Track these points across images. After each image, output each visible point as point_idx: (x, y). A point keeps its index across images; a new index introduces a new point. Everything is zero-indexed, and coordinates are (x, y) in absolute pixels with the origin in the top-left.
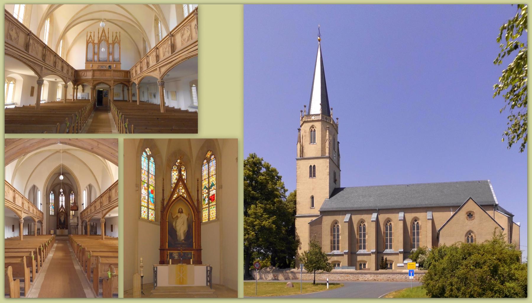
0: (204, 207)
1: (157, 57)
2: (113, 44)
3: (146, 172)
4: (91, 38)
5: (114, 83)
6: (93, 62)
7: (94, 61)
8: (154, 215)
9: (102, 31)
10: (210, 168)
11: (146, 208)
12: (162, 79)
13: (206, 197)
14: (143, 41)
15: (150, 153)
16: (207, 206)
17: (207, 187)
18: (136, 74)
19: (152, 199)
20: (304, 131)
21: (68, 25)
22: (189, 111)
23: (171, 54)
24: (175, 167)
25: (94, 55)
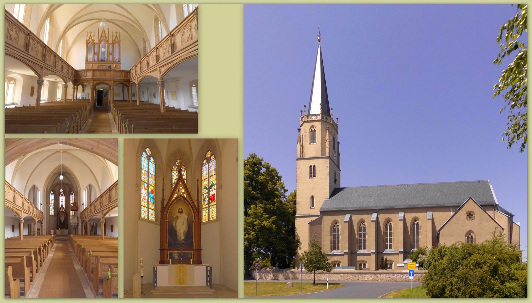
0: (204, 207)
1: (157, 57)
2: (113, 44)
3: (146, 172)
4: (91, 38)
5: (114, 83)
6: (93, 62)
7: (94, 61)
8: (154, 215)
9: (102, 31)
10: (210, 168)
11: (146, 208)
12: (162, 79)
13: (206, 197)
14: (143, 41)
15: (150, 153)
16: (207, 206)
17: (207, 187)
18: (136, 74)
19: (152, 199)
20: (304, 131)
21: (68, 25)
22: (189, 111)
23: (171, 54)
24: (175, 167)
25: (94, 55)
